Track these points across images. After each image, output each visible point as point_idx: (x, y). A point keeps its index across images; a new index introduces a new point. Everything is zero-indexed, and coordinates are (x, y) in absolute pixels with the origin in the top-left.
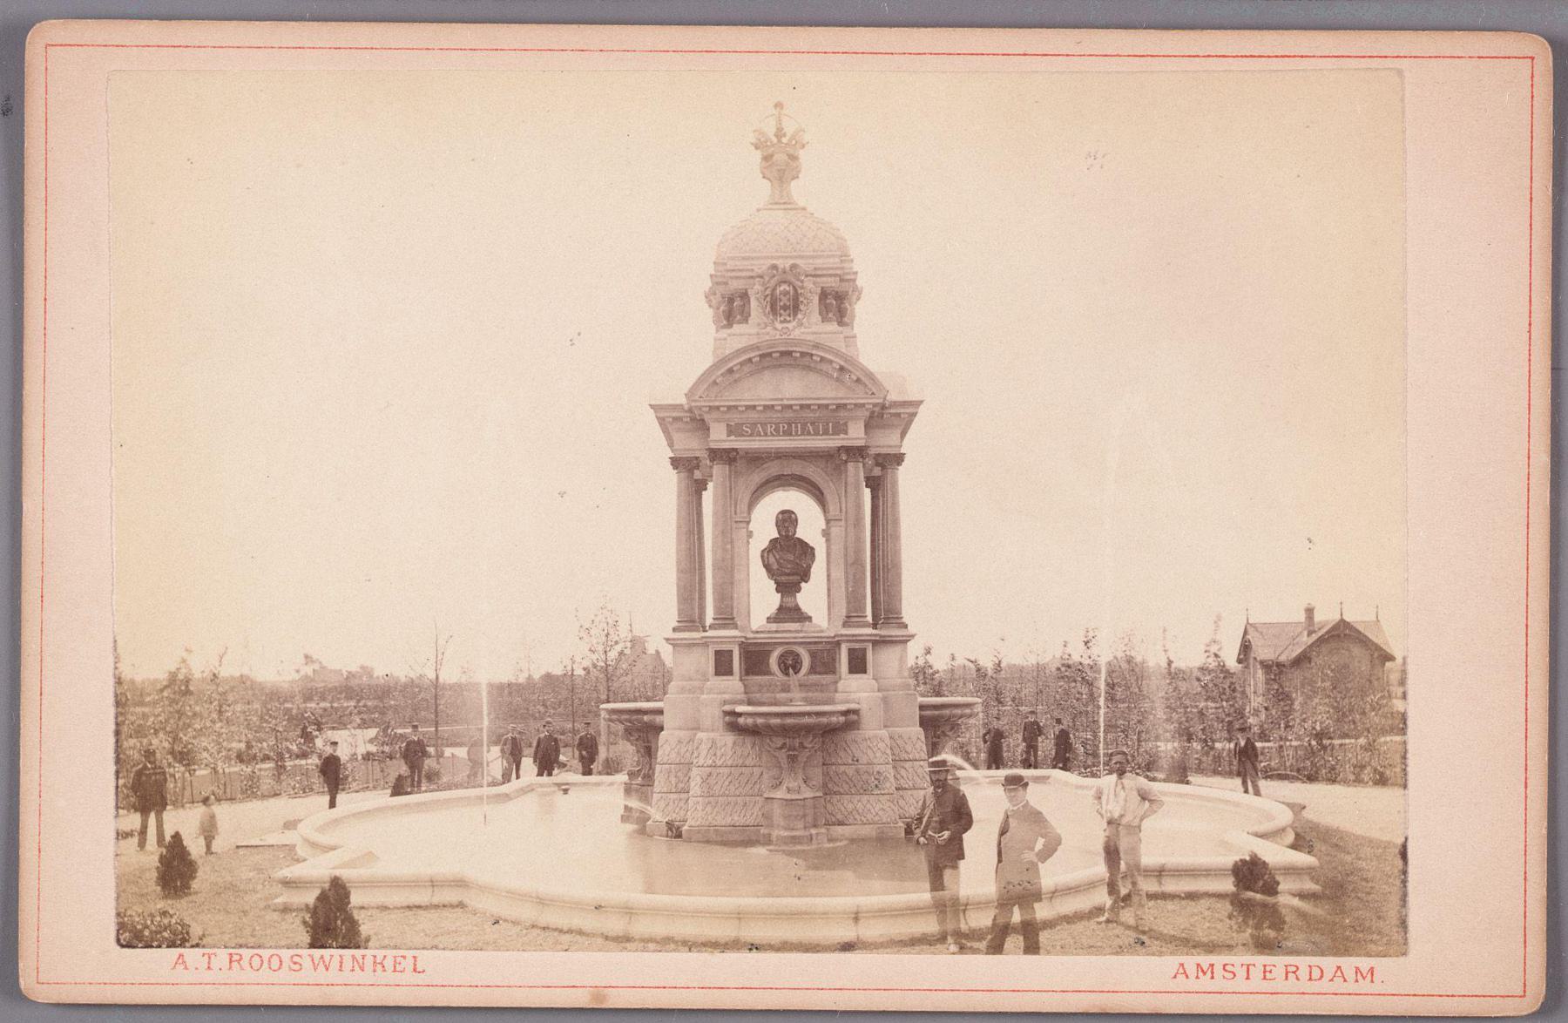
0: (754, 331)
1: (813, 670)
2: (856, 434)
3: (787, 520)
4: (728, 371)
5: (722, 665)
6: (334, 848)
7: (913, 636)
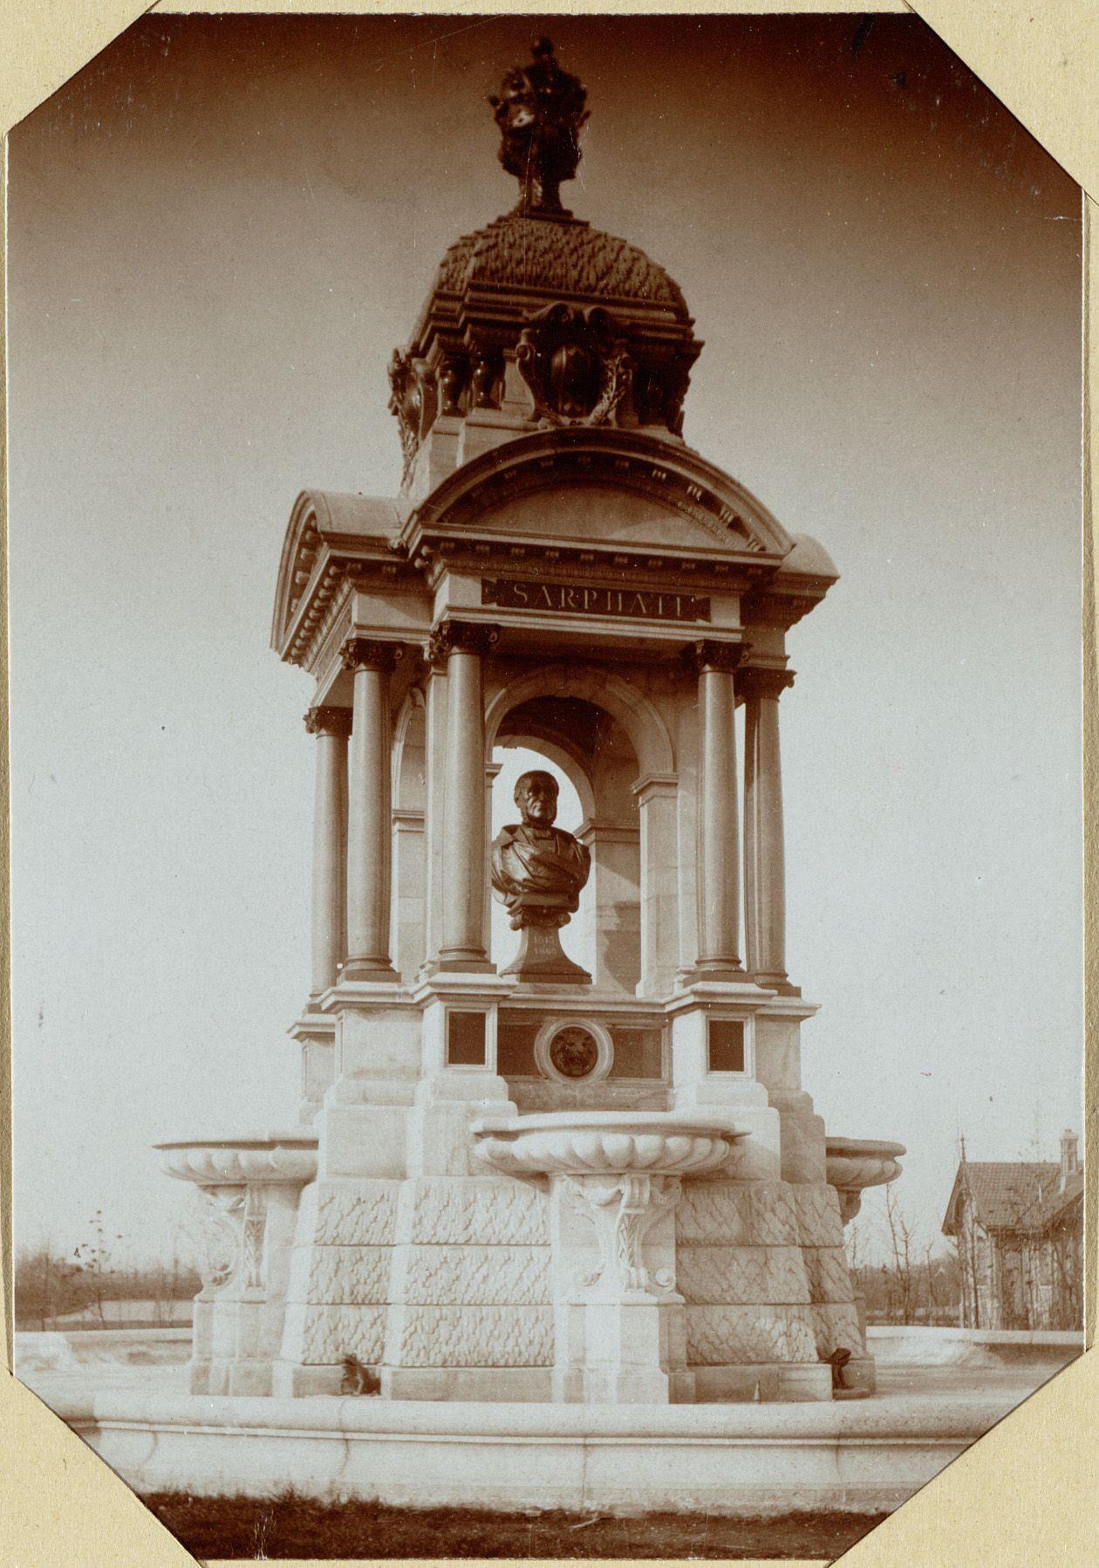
0: (515, 410)
1: (616, 1071)
2: (725, 621)
3: (541, 786)
5: (463, 1042)
6: (480, 1135)
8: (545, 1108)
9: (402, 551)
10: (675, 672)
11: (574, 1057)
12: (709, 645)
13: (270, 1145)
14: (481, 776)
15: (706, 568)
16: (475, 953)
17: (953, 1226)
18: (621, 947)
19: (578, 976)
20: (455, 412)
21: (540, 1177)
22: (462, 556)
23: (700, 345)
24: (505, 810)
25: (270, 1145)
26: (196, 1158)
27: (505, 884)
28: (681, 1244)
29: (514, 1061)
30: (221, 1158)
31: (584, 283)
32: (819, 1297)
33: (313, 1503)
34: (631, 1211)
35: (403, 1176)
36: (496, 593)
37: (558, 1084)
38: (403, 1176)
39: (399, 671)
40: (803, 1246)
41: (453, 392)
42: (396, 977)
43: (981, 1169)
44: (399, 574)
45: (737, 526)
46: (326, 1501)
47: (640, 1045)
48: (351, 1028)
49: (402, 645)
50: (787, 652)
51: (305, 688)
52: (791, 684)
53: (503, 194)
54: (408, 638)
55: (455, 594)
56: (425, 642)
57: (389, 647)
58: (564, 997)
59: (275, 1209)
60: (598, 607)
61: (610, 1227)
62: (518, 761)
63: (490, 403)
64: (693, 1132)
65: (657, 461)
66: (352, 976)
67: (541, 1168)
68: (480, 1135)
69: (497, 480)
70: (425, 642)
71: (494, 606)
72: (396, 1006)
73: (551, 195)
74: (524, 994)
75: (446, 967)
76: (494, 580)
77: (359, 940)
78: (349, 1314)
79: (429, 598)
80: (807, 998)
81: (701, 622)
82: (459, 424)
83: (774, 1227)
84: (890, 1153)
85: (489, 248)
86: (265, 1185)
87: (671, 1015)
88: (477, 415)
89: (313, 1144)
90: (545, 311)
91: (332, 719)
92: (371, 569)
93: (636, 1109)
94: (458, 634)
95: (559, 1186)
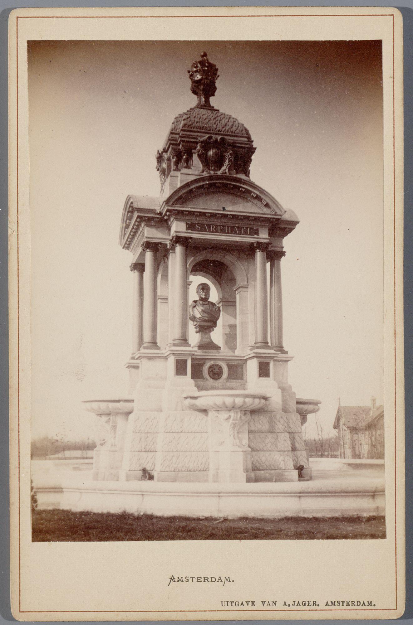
0: (196, 169)
2: (264, 236)
5: (180, 368)
6: (186, 398)
7: (292, 358)
8: (206, 389)
9: (160, 214)
10: (249, 251)
11: (215, 373)
12: (259, 243)
13: (119, 401)
14: (186, 285)
15: (256, 219)
16: (184, 340)
17: (336, 426)
18: (231, 338)
19: (217, 348)
20: (177, 170)
21: (205, 411)
22: (180, 215)
23: (255, 149)
24: (193, 295)
25: (119, 401)
26: (95, 405)
27: (193, 319)
28: (250, 432)
29: (197, 374)
30: (103, 405)
31: (218, 129)
32: (294, 449)
33: (132, 515)
34: (234, 422)
35: (161, 411)
36: (191, 227)
37: (211, 382)
38: (161, 411)
39: (159, 251)
40: (289, 433)
41: (177, 164)
42: (159, 348)
43: (345, 408)
44: (161, 221)
45: (267, 205)
46: (136, 514)
47: (236, 370)
48: (145, 364)
49: (161, 243)
50: (283, 246)
51: (131, 257)
52: (284, 255)
53: (192, 101)
54: (163, 241)
55: (178, 227)
56: (168, 242)
57: (156, 244)
58: (212, 354)
59: (120, 420)
60: (223, 231)
61: (227, 427)
62: (197, 280)
63: (188, 167)
64: (254, 397)
65: (242, 185)
66: (145, 348)
67: (204, 408)
68: (186, 398)
69: (191, 191)
70: (168, 242)
71: (190, 231)
72: (159, 357)
73: (207, 101)
74: (199, 353)
75: (174, 345)
76: (190, 223)
77: (147, 337)
78: (144, 455)
79: (169, 228)
80: (290, 354)
81: (256, 236)
82: (178, 174)
83: (280, 426)
84: (316, 403)
85: (188, 118)
86: (117, 414)
87: (246, 360)
88: (184, 171)
89: (133, 401)
90: (205, 138)
91: (139, 267)
92: (150, 219)
93: (235, 389)
94: (178, 240)
95: (211, 414)
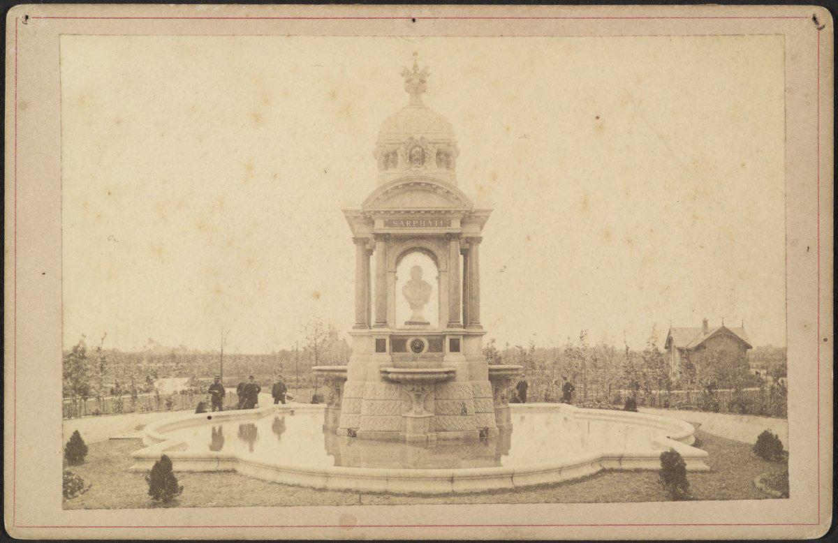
0: (402, 171)
1: (430, 350)
2: (455, 227)
3: (417, 270)
4: (389, 192)
5: (380, 347)
36: (389, 224)
71: (387, 228)
81: (448, 227)
94: (378, 236)
